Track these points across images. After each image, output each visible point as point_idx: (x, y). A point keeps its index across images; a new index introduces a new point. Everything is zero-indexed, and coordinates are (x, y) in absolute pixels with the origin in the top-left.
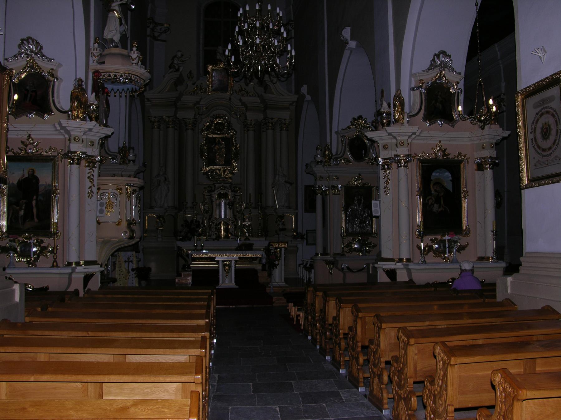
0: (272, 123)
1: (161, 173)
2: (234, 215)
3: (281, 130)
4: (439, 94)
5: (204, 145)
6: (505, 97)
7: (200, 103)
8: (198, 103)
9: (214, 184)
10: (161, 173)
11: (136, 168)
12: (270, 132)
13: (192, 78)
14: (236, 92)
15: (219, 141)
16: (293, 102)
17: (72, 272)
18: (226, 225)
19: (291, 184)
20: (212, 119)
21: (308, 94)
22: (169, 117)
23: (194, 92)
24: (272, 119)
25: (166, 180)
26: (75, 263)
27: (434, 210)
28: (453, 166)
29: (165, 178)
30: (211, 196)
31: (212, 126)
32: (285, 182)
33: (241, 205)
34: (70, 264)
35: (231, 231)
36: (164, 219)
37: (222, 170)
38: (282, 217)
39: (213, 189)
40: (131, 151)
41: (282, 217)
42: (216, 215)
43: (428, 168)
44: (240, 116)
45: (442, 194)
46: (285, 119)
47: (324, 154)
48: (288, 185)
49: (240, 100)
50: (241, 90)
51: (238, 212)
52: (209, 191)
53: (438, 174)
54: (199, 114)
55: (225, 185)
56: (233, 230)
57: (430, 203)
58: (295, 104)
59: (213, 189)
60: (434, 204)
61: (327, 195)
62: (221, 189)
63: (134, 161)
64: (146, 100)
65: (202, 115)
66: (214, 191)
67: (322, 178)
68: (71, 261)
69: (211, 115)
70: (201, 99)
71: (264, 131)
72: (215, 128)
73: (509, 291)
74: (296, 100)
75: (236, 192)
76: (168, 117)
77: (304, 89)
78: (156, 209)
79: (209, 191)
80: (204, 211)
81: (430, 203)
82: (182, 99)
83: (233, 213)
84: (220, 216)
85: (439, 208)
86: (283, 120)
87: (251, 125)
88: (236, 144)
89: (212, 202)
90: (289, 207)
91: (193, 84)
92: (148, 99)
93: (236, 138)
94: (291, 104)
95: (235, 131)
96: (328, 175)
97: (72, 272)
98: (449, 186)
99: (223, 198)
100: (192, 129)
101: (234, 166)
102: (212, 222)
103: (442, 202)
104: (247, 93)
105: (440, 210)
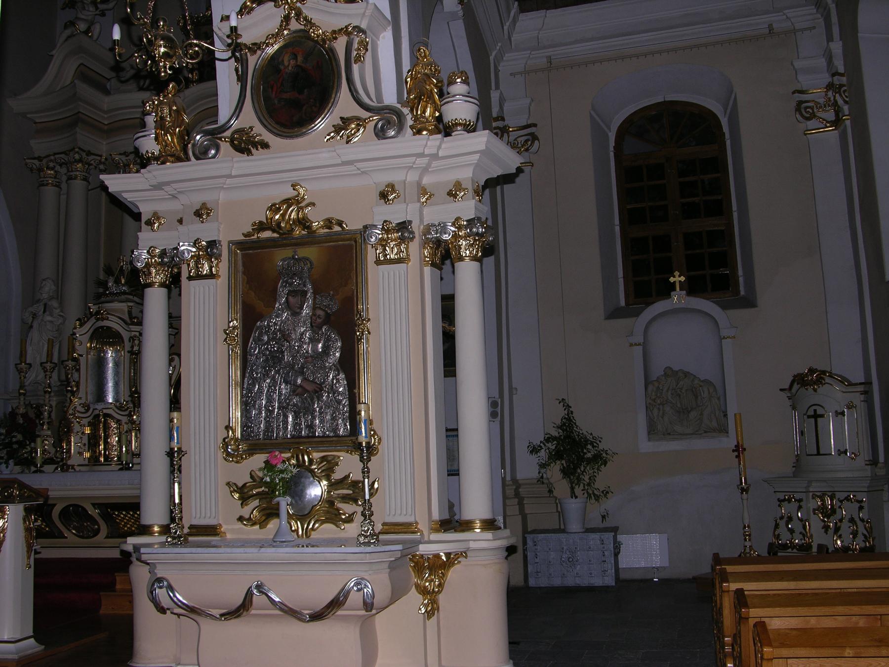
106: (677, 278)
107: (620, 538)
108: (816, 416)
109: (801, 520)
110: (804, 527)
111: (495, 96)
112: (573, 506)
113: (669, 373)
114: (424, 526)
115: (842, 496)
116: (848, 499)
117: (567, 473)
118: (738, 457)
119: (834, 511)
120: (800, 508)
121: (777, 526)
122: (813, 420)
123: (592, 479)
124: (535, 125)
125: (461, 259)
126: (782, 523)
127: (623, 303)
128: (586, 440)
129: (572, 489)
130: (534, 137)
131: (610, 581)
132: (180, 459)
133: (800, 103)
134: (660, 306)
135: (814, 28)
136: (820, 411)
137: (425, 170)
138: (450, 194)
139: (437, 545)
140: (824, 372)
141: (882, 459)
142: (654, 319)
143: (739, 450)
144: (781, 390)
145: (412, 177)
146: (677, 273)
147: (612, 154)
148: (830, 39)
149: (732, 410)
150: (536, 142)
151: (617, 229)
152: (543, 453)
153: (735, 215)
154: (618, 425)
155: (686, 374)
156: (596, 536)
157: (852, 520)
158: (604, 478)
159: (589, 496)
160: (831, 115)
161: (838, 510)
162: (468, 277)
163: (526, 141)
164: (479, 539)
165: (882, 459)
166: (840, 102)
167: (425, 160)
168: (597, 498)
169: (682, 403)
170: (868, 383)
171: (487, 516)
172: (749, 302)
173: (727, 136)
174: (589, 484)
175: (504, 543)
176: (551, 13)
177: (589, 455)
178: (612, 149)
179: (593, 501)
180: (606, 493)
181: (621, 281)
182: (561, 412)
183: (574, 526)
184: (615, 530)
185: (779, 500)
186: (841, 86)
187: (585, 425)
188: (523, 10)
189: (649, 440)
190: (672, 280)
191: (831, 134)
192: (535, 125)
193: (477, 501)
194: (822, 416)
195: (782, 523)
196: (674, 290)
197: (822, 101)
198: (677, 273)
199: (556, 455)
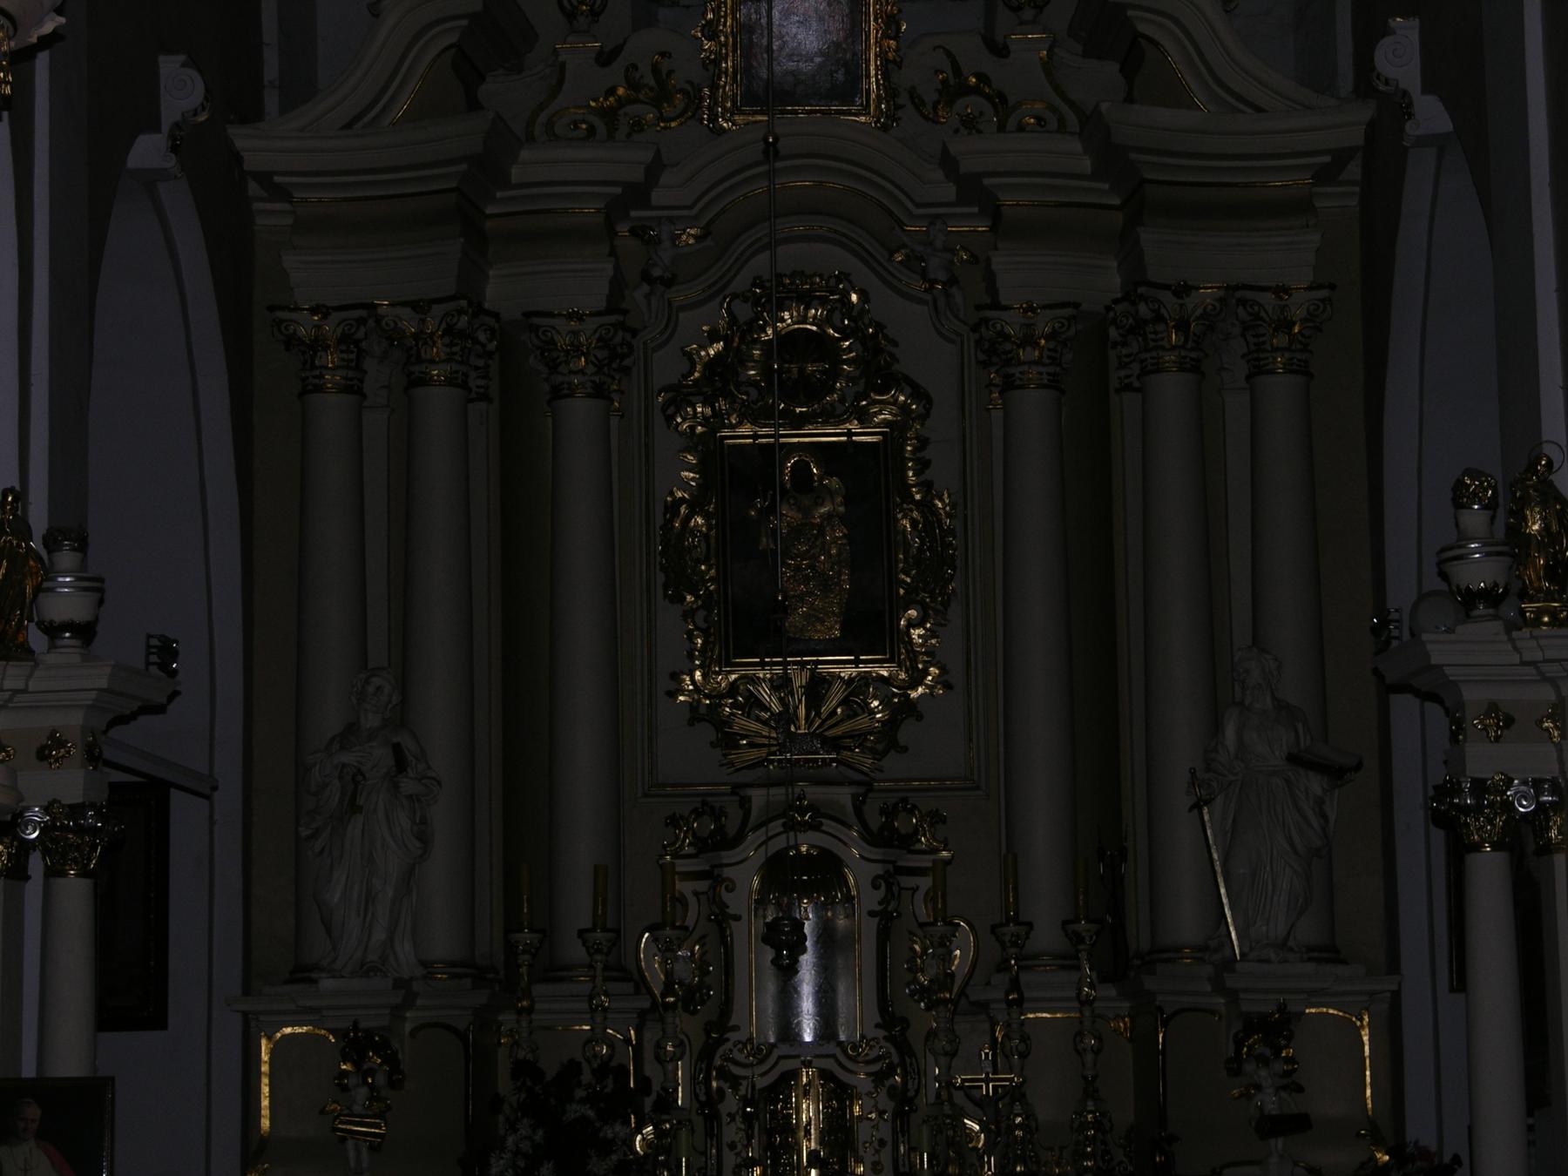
0: (1182, 326)
1: (371, 721)
2: (891, 1021)
3: (1258, 369)
5: (695, 506)
7: (657, 197)
8: (637, 194)
9: (736, 788)
10: (371, 721)
11: (98, 678)
12: (1171, 389)
13: (595, 14)
14: (917, 101)
15: (801, 470)
16: (1341, 157)
18: (837, 1093)
19: (1336, 774)
20: (744, 312)
21: (1426, 89)
22: (419, 307)
23: (610, 115)
24: (1183, 290)
25: (401, 764)
29: (397, 750)
30: (712, 875)
31: (743, 360)
32: (1293, 759)
33: (945, 945)
35: (863, 1133)
36: (392, 1060)
37: (800, 680)
38: (1276, 1028)
39: (732, 829)
40: (66, 558)
41: (1276, 1028)
42: (755, 1015)
44: (952, 281)
46: (1282, 290)
47: (1516, 533)
48: (1315, 784)
49: (948, 162)
50: (953, 91)
51: (923, 992)
52: (704, 845)
54: (646, 277)
55: (814, 793)
56: (885, 1132)
58: (1354, 170)
59: (732, 829)
61: (1547, 849)
62: (791, 827)
63: (85, 632)
64: (253, 188)
65: (669, 282)
66: (739, 839)
67: (1509, 721)
69: (741, 282)
70: (655, 169)
71: (1128, 388)
72: (766, 372)
73: (265, 1123)
74: (1357, 137)
75: (907, 842)
76: (415, 305)
77: (1401, 55)
78: (327, 984)
79: (704, 845)
80: (668, 989)
82: (516, 173)
83: (883, 1002)
84: (789, 1031)
86: (1268, 299)
87: (1029, 341)
88: (926, 487)
89: (722, 919)
90: (1329, 953)
91: (605, 59)
92: (264, 178)
93: (923, 443)
94: (1326, 175)
95: (918, 393)
96: (1548, 694)
99: (806, 890)
100: (599, 392)
101: (913, 655)
102: (724, 1074)
104: (1000, 101)
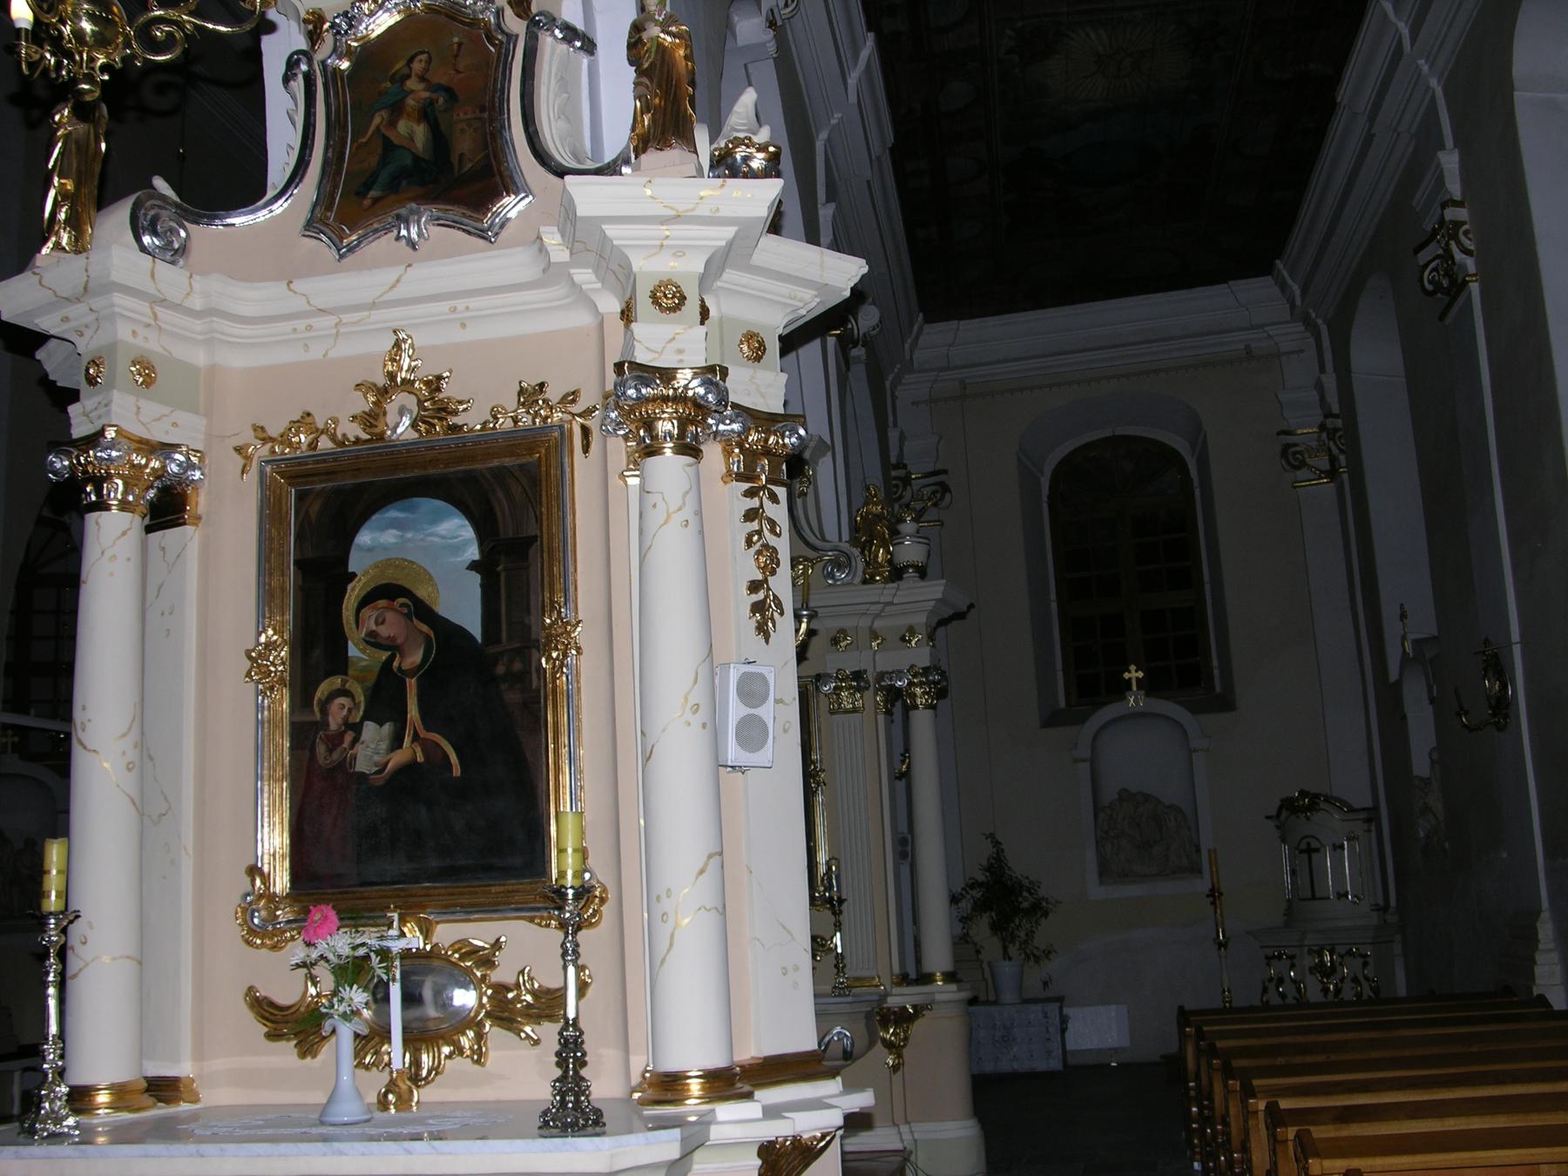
4: (417, 66)
6: (1462, 214)
17: (687, 1154)
26: (943, 974)
27: (363, 765)
28: (510, 492)
34: (668, 1086)
43: (325, 503)
45: (415, 658)
53: (390, 537)
57: (334, 723)
60: (357, 728)
68: (671, 1065)
81: (334, 723)
85: (397, 742)
97: (687, 1154)
98: (463, 605)
103: (413, 711)
105: (399, 758)
106: (1134, 674)
107: (1066, 1011)
108: (1310, 851)
109: (1293, 981)
110: (1299, 989)
111: (893, 435)
112: (1007, 970)
113: (1125, 796)
114: (886, 980)
115: (1342, 950)
116: (1350, 953)
117: (996, 927)
118: (1213, 903)
119: (1333, 969)
120: (1292, 967)
121: (1265, 990)
122: (1305, 856)
123: (1030, 934)
124: (945, 472)
125: (916, 707)
126: (1272, 987)
127: (1062, 704)
128: (1021, 886)
129: (1005, 949)
130: (945, 489)
131: (1055, 1064)
132: (64, 931)
133: (1287, 447)
134: (1110, 711)
135: (1302, 351)
136: (1315, 844)
137: (877, 616)
138: (903, 639)
139: (902, 998)
140: (1317, 796)
141: (1393, 902)
142: (1104, 727)
143: (1214, 894)
144: (1268, 818)
145: (864, 623)
146: (1133, 668)
147: (1045, 507)
148: (1322, 370)
149: (1206, 843)
150: (948, 495)
151: (1054, 605)
152: (963, 904)
153: (1207, 587)
154: (1061, 864)
155: (1147, 798)
156: (1038, 1008)
157: (1355, 980)
158: (1045, 933)
159: (1028, 957)
160: (1323, 462)
161: (1339, 968)
162: (922, 722)
163: (934, 493)
164: (941, 990)
165: (1393, 902)
166: (1335, 451)
167: (880, 607)
168: (1037, 960)
169: (1143, 836)
170: (1375, 809)
171: (948, 967)
172: (1225, 703)
173: (1196, 483)
174: (1026, 942)
175: (964, 995)
176: (964, 324)
177: (1025, 905)
178: (1045, 499)
179: (1032, 963)
180: (1048, 953)
181: (1060, 675)
182: (988, 850)
183: (1009, 996)
184: (1060, 1000)
185: (1267, 958)
186: (1336, 430)
187: (1019, 866)
188: (927, 321)
189: (1101, 883)
190: (1126, 675)
191: (1326, 487)
192: (945, 472)
193: (938, 957)
194: (1317, 850)
195: (1272, 987)
196: (1130, 688)
197: (1314, 444)
198: (1133, 668)
199: (981, 907)
